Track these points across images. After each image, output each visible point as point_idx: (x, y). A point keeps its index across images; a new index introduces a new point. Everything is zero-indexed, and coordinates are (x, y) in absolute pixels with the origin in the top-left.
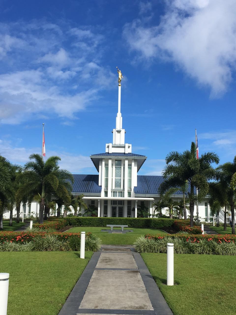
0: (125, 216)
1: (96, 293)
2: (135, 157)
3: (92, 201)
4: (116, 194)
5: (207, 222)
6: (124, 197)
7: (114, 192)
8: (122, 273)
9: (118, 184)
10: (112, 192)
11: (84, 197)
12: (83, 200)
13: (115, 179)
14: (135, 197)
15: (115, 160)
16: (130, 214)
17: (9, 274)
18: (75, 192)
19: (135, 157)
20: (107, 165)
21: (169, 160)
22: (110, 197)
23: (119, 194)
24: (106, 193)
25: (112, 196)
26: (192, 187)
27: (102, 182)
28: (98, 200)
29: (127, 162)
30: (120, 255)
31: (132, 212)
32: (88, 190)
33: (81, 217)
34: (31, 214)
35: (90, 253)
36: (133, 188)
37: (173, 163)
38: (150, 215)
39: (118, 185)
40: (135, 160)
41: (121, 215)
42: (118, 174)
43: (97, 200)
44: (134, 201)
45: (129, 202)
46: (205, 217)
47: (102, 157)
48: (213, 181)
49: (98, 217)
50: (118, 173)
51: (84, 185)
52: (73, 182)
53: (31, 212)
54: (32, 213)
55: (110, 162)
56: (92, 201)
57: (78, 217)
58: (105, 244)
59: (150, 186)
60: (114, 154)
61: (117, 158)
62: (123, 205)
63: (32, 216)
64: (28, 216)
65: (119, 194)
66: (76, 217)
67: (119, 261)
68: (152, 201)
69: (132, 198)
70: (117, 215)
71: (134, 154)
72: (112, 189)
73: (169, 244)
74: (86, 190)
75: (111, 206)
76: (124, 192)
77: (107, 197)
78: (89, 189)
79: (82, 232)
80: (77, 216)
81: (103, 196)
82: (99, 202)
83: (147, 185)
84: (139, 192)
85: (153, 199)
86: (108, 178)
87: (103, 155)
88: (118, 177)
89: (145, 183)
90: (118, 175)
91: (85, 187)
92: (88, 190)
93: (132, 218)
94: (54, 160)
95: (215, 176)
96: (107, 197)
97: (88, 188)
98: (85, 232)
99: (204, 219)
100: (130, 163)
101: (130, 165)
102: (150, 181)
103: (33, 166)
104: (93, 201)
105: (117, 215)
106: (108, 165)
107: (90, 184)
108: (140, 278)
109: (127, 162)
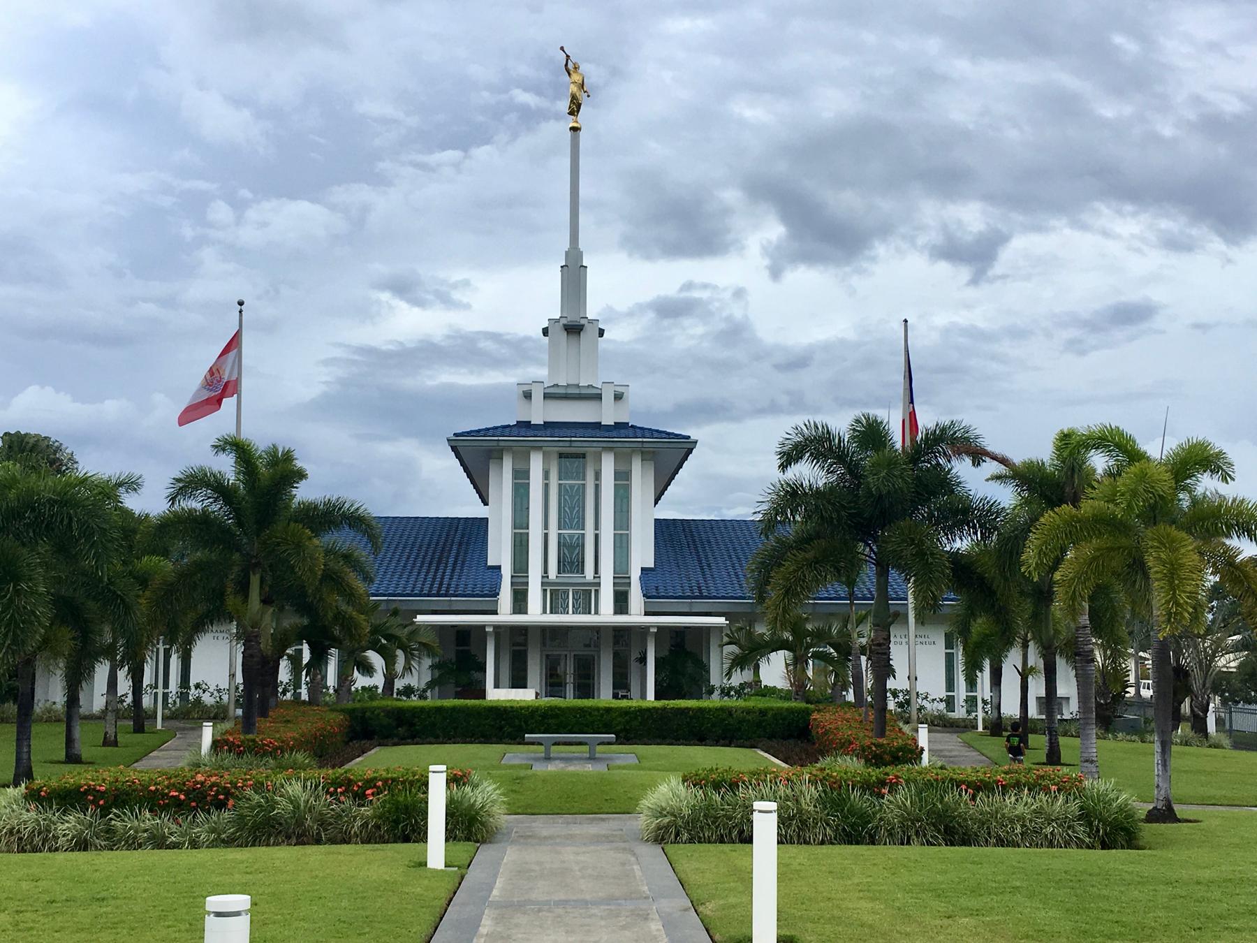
0: (605, 696)
1: (558, 841)
2: (645, 440)
3: (458, 632)
4: (564, 601)
5: (951, 714)
6: (597, 613)
7: (555, 599)
8: (590, 917)
9: (571, 558)
10: (545, 591)
11: (420, 618)
12: (418, 629)
13: (559, 538)
14: (647, 614)
15: (556, 456)
16: (627, 687)
17: (207, 909)
18: (384, 595)
19: (645, 440)
20: (521, 476)
21: (789, 457)
22: (536, 613)
23: (577, 600)
24: (520, 600)
25: (544, 612)
26: (883, 573)
27: (500, 552)
28: (483, 627)
29: (608, 466)
30: (584, 853)
31: (634, 667)
32: (441, 584)
33: (414, 701)
34: (193, 693)
35: (463, 849)
36: (635, 575)
37: (808, 473)
38: (711, 691)
39: (573, 563)
40: (648, 455)
41: (586, 688)
42: (572, 514)
43: (481, 628)
44: (642, 631)
45: (621, 635)
46: (943, 694)
47: (502, 444)
48: (962, 544)
49: (484, 697)
50: (572, 509)
51: (423, 563)
52: (376, 549)
53: (191, 684)
54: (198, 686)
55: (536, 465)
56: (458, 632)
57: (399, 704)
58: (520, 811)
59: (709, 566)
60: (550, 427)
61: (567, 444)
62: (592, 648)
63: (198, 700)
64: (178, 701)
65: (577, 600)
66: (388, 703)
67: (578, 873)
68: (719, 629)
69: (636, 615)
70: (570, 690)
71: (639, 428)
72: (546, 580)
73: (758, 805)
74: (432, 585)
75: (541, 651)
76: (597, 592)
77: (526, 613)
78: (446, 581)
79: (432, 768)
80: (397, 700)
81: (505, 615)
82: (488, 638)
83: (700, 561)
84: (662, 590)
85: (721, 620)
86: (528, 533)
87: (507, 434)
88: (571, 528)
89: (686, 551)
90: (571, 520)
91: (421, 567)
92: (441, 584)
93: (634, 703)
94: (296, 459)
95: (974, 527)
96: (526, 613)
97: (442, 579)
98: (444, 768)
99: (941, 700)
100: (622, 468)
101: (622, 477)
102: (709, 542)
103: (208, 485)
104: (463, 635)
105: (570, 690)
106: (528, 478)
107: (451, 560)
108: (658, 930)
109: (608, 466)
